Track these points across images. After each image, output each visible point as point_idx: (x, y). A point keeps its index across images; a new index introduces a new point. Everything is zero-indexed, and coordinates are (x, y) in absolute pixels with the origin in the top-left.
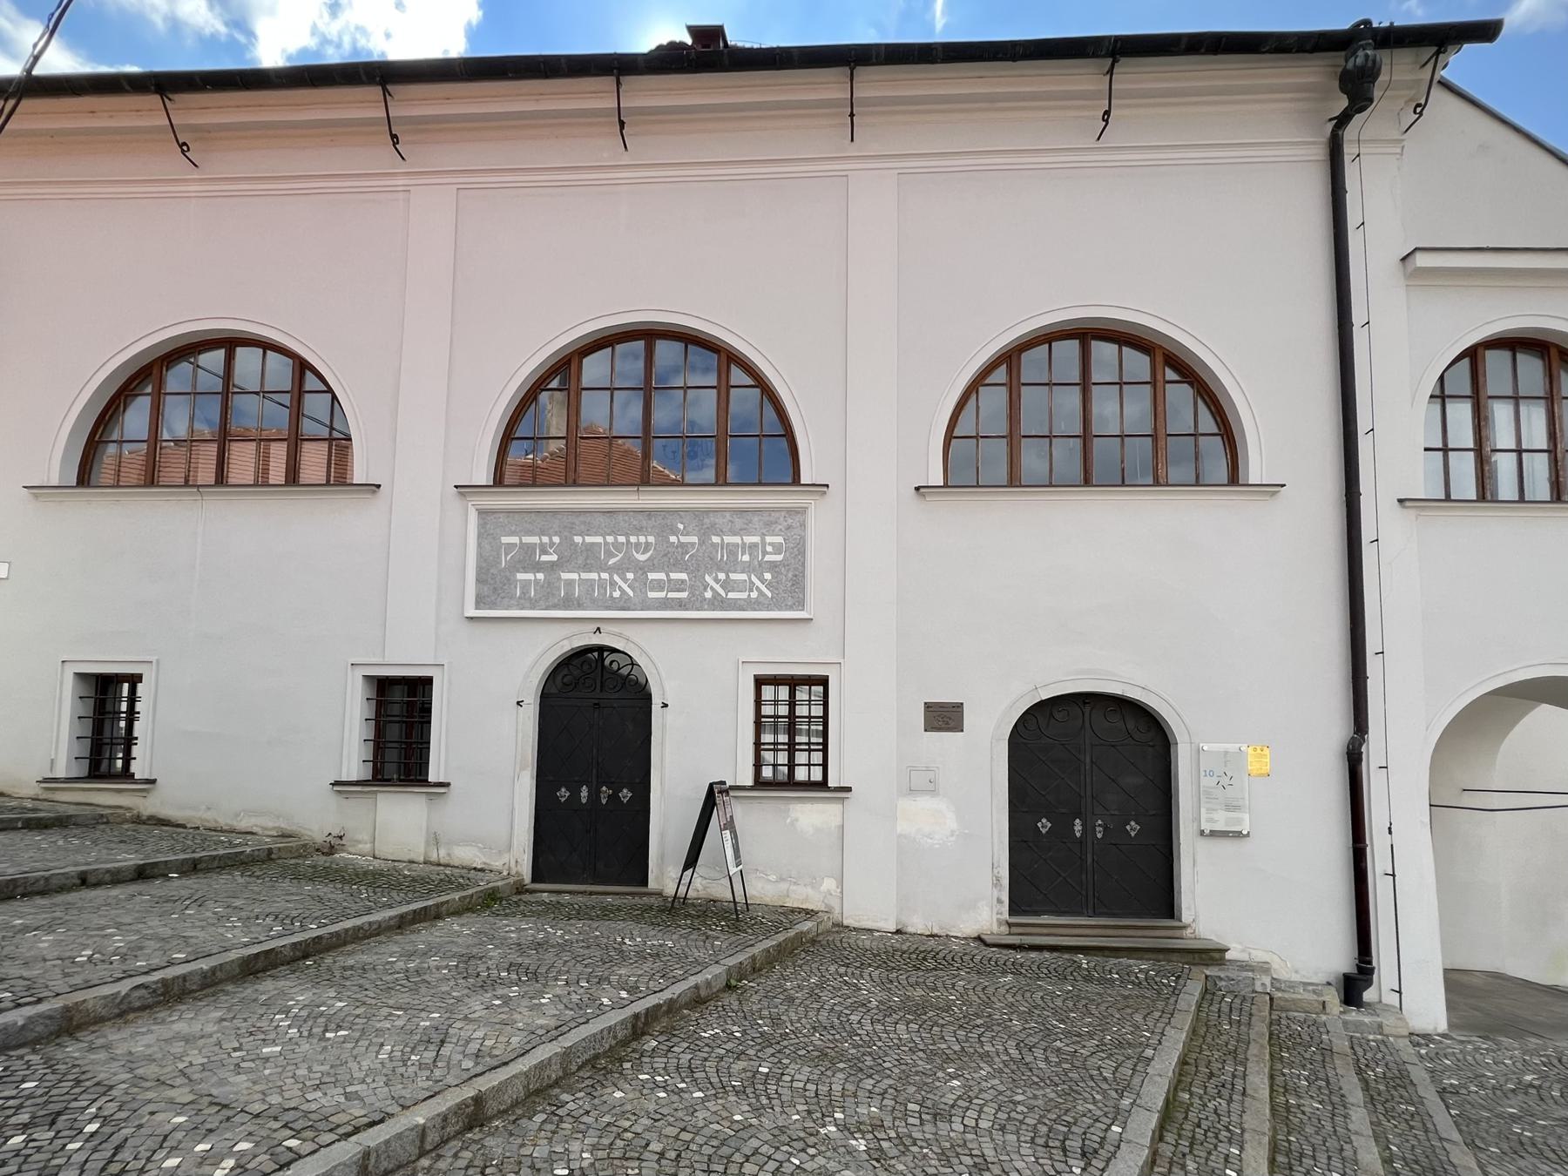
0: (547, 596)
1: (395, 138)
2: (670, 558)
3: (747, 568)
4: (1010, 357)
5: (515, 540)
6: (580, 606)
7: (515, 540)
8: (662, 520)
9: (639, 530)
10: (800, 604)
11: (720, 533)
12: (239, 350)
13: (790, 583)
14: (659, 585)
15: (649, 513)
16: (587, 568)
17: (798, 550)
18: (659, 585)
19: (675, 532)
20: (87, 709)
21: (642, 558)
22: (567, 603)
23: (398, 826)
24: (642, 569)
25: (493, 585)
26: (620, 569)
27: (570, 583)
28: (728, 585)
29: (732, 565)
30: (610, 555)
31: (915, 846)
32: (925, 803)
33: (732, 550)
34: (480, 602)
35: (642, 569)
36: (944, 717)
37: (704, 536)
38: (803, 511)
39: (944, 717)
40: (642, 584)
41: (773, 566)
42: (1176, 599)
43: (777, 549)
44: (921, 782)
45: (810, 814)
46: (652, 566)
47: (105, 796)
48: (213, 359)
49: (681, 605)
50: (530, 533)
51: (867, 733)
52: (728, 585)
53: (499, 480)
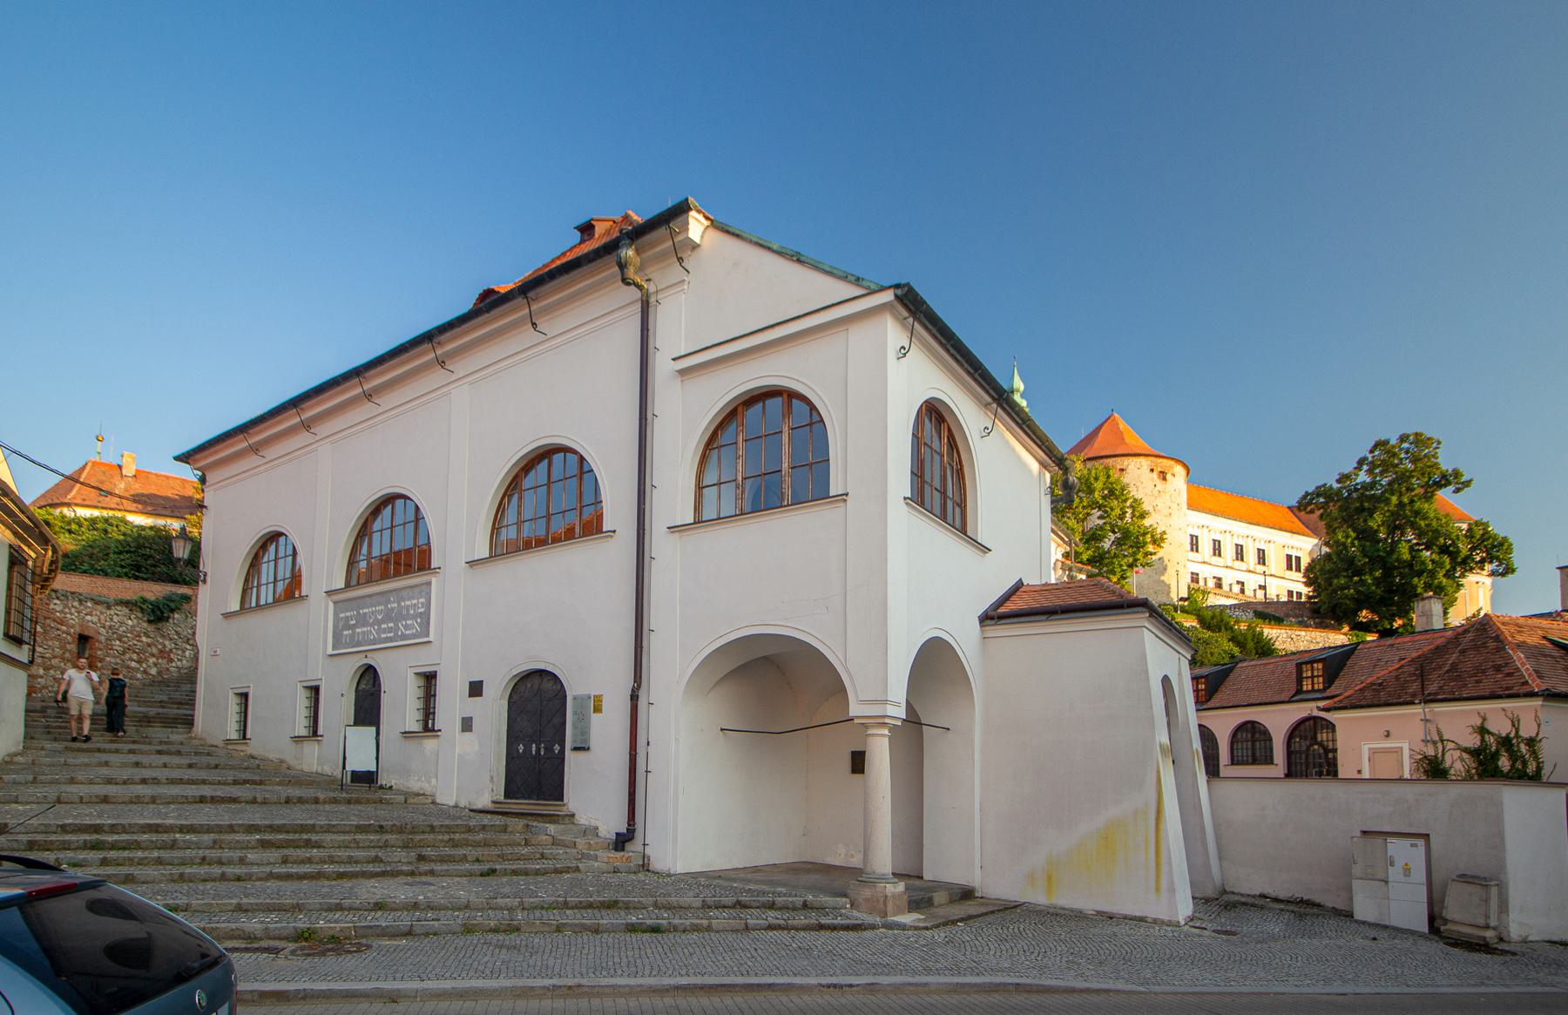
26: (372, 625)
28: (407, 627)
31: (462, 766)
33: (408, 607)
34: (334, 647)
38: (429, 584)
40: (379, 631)
42: (559, 609)
45: (430, 744)
46: (383, 621)
48: (387, 511)
52: (407, 627)
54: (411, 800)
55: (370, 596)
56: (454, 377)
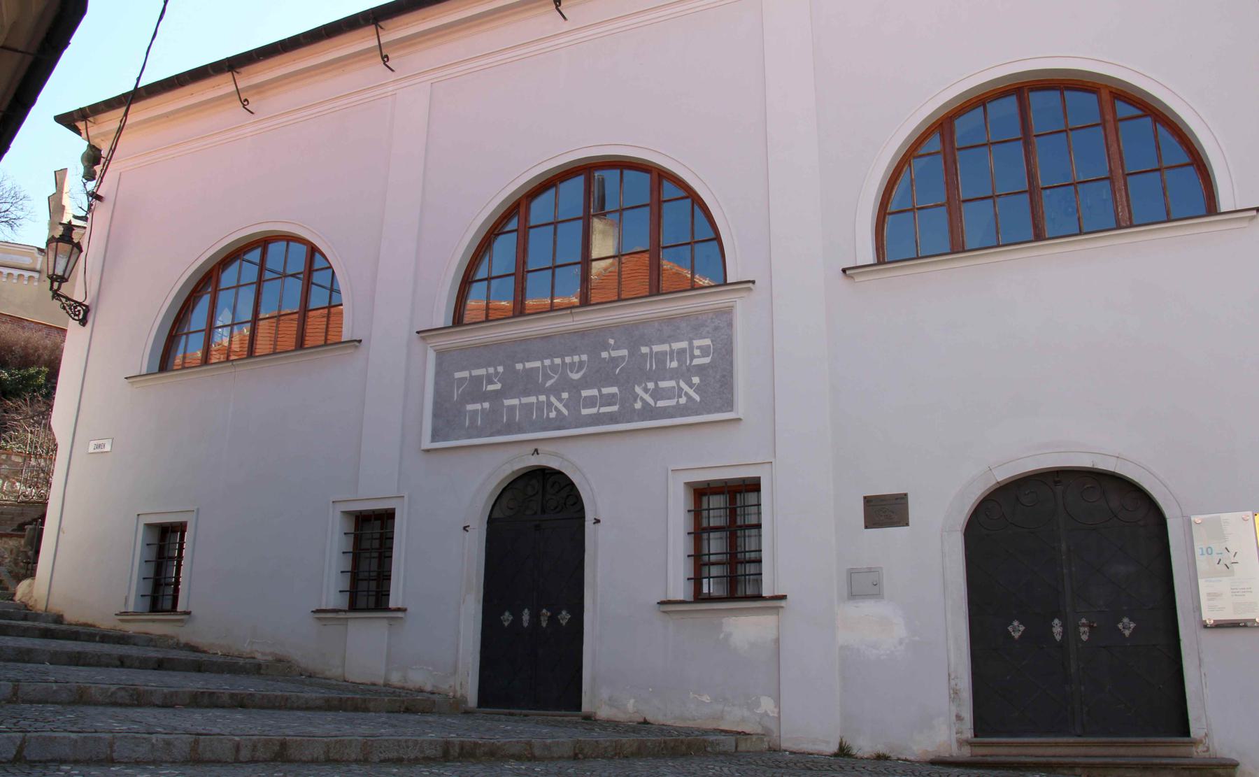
0: (495, 423)
1: (385, 58)
2: (601, 374)
3: (675, 374)
4: (515, 213)
5: (465, 374)
6: (521, 430)
7: (465, 374)
8: (593, 339)
9: (574, 351)
10: (729, 405)
11: (649, 343)
12: (292, 244)
13: (718, 386)
14: (591, 402)
15: (582, 333)
16: (527, 393)
17: (725, 352)
18: (591, 402)
19: (606, 347)
20: (152, 554)
21: (576, 376)
22: (510, 428)
23: (365, 651)
24: (575, 387)
25: (447, 418)
26: (556, 391)
27: (512, 408)
28: (657, 394)
29: (662, 373)
30: (547, 377)
32: (868, 608)
33: (661, 358)
34: (434, 438)
35: (575, 387)
36: (885, 511)
37: (633, 351)
39: (885, 511)
41: (701, 370)
43: (705, 351)
44: (863, 585)
45: (744, 628)
46: (585, 383)
47: (157, 626)
48: (255, 255)
49: (612, 418)
50: (478, 366)
51: (799, 538)
52: (657, 394)
53: (458, 319)
54: (742, 747)
55: (462, 349)
56: (566, 26)
